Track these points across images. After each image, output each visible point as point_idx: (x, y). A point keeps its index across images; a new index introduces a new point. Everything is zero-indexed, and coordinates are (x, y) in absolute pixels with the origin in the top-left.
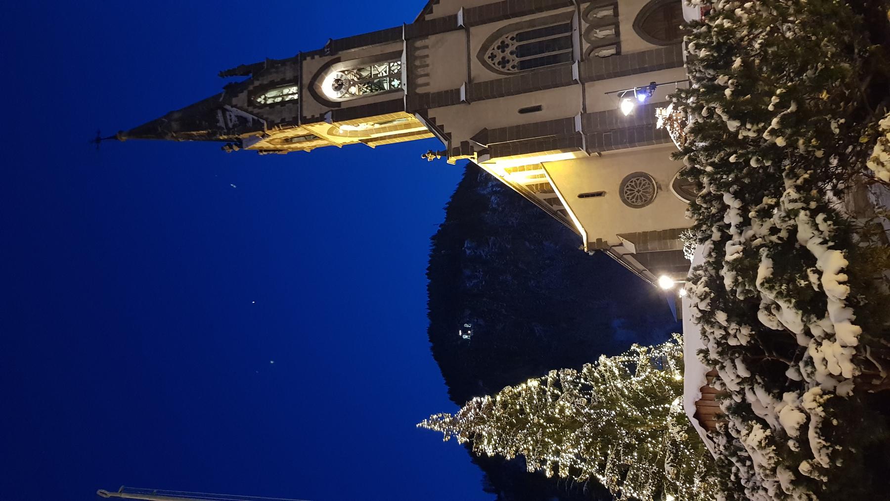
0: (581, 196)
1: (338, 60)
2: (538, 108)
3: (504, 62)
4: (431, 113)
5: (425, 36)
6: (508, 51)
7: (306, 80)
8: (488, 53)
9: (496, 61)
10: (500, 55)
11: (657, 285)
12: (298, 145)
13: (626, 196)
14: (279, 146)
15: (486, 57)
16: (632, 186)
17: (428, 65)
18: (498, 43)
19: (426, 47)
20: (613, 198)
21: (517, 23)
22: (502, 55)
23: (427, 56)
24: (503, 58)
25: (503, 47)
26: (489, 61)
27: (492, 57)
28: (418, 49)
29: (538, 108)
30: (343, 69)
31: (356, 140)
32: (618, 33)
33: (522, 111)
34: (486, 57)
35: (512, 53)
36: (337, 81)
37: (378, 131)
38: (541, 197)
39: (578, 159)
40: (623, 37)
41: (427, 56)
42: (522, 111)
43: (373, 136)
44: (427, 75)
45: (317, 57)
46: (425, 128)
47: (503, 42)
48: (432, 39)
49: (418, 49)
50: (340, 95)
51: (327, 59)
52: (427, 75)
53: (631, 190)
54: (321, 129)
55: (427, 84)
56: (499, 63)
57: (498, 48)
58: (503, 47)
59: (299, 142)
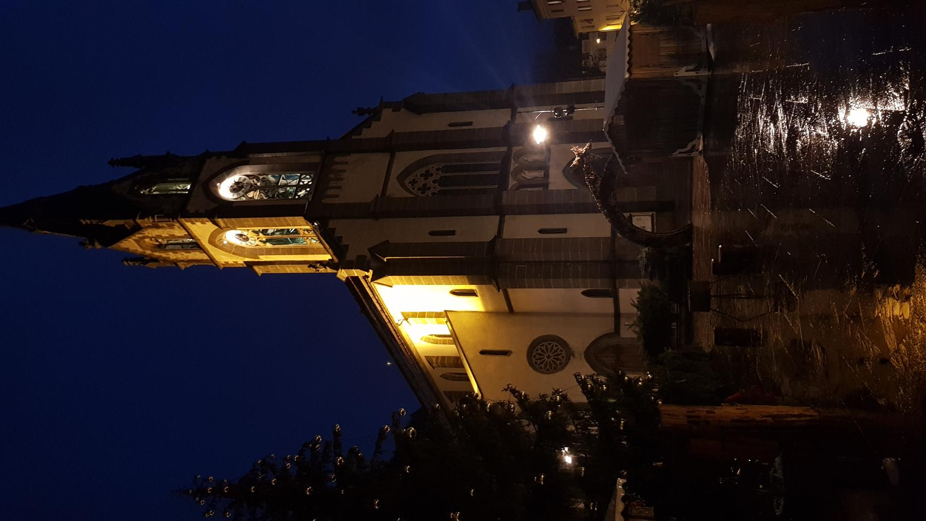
0: (483, 352)
1: (246, 163)
2: (453, 233)
3: (424, 189)
4: (332, 224)
5: (348, 153)
6: (431, 179)
7: (203, 176)
8: (411, 178)
9: (416, 186)
10: (421, 182)
11: (548, 138)
12: (172, 256)
13: (534, 360)
14: (148, 252)
15: (407, 182)
16: (543, 351)
17: (342, 179)
18: (423, 170)
19: (346, 163)
20: (520, 357)
21: (445, 155)
22: (424, 182)
23: (344, 171)
24: (425, 185)
25: (427, 175)
26: (409, 186)
27: (413, 182)
28: (338, 163)
29: (453, 233)
30: (249, 173)
31: (241, 261)
32: (547, 175)
33: (432, 233)
34: (407, 182)
35: (434, 182)
36: (237, 183)
37: (269, 252)
38: (444, 386)
39: (487, 312)
40: (552, 179)
41: (344, 171)
42: (432, 233)
43: (263, 258)
44: (339, 188)
45: (224, 158)
46: (327, 257)
47: (427, 171)
48: (354, 157)
49: (338, 163)
50: (236, 197)
51: (235, 160)
52: (339, 188)
53: (540, 354)
54: (202, 229)
55: (337, 196)
56: (419, 189)
57: (421, 175)
58: (427, 175)
59: (174, 251)
